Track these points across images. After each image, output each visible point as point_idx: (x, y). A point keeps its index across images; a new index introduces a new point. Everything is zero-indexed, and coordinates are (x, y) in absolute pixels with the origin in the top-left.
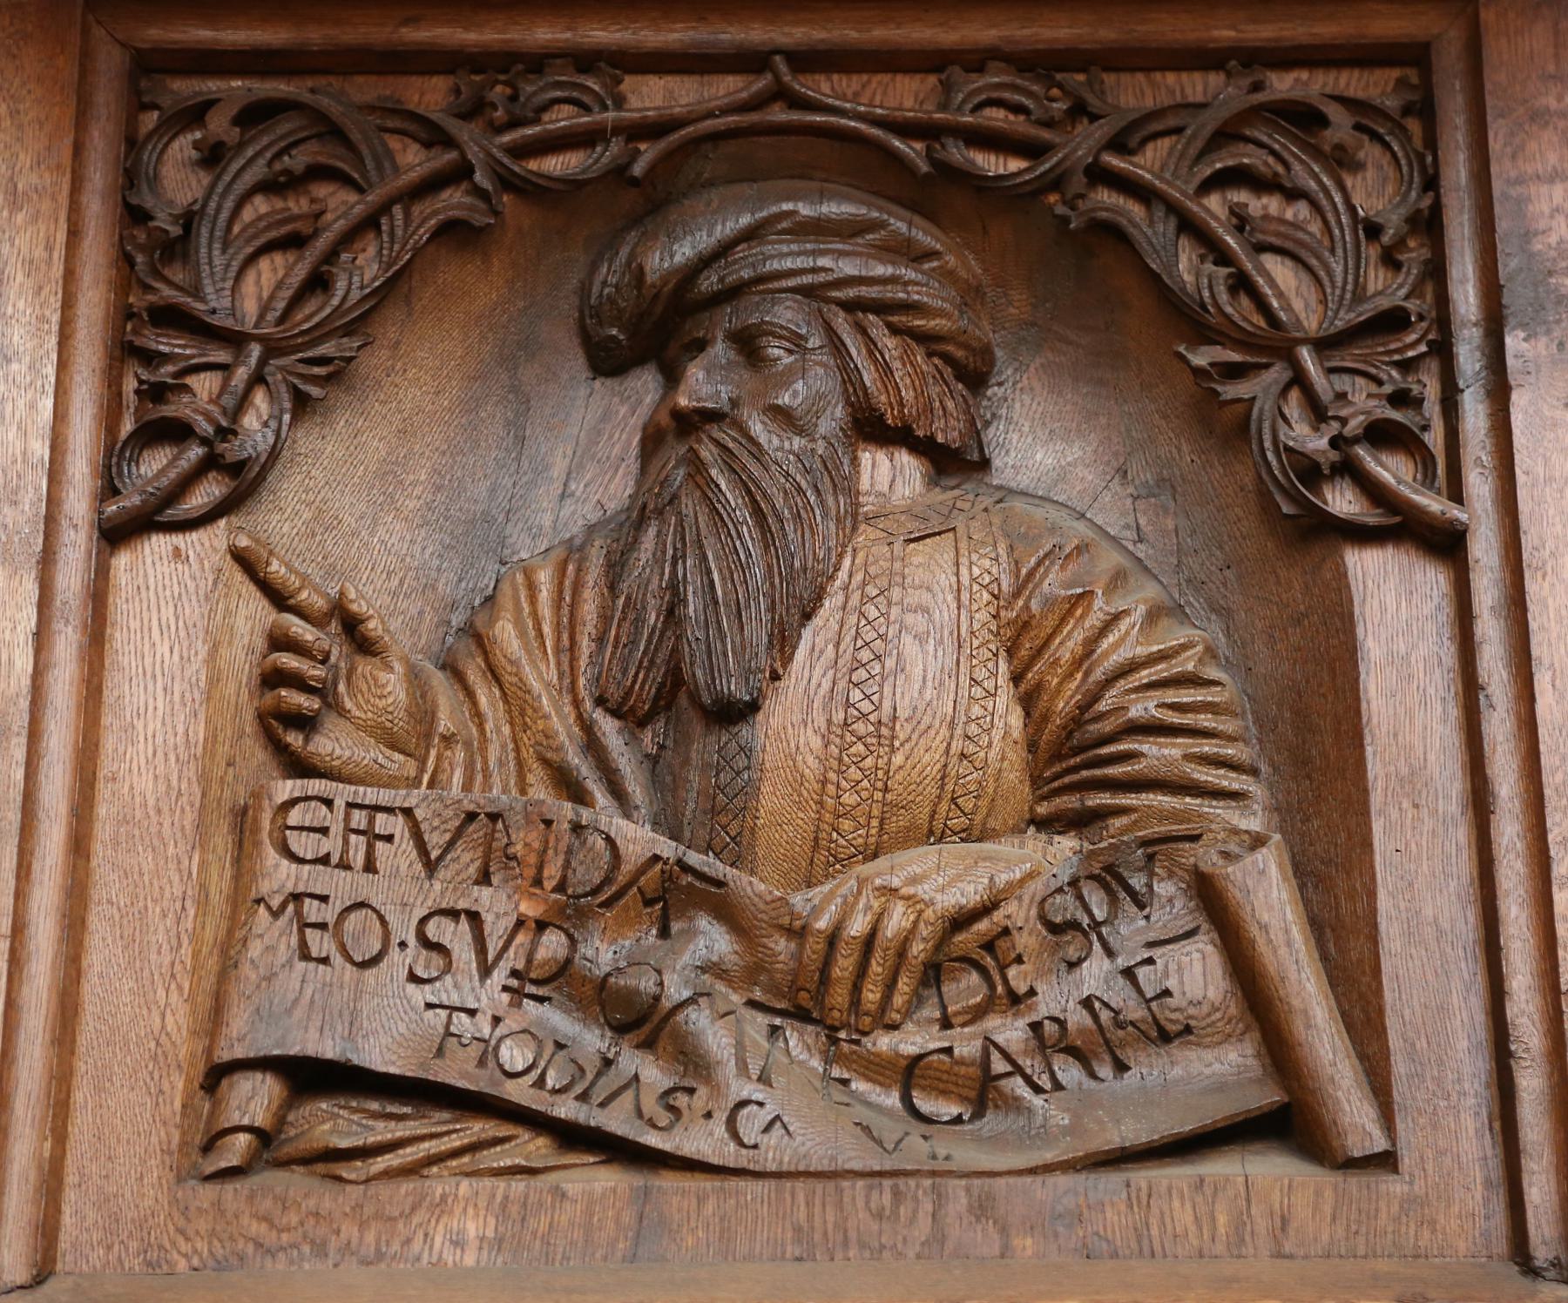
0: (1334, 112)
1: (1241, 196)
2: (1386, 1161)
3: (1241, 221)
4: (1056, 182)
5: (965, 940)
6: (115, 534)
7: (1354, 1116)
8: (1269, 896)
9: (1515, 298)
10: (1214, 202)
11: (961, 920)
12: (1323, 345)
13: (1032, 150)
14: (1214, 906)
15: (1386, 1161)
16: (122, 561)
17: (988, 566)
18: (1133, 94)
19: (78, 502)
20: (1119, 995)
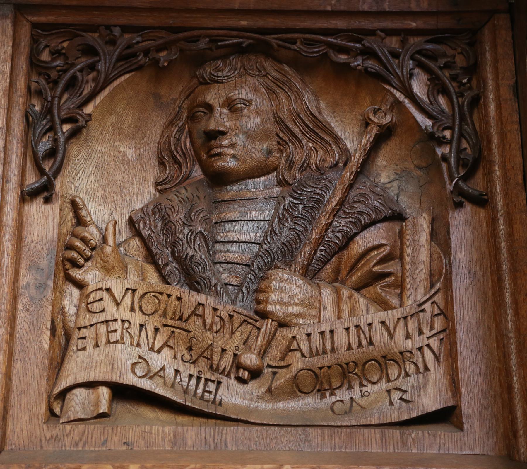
16: (27, 207)
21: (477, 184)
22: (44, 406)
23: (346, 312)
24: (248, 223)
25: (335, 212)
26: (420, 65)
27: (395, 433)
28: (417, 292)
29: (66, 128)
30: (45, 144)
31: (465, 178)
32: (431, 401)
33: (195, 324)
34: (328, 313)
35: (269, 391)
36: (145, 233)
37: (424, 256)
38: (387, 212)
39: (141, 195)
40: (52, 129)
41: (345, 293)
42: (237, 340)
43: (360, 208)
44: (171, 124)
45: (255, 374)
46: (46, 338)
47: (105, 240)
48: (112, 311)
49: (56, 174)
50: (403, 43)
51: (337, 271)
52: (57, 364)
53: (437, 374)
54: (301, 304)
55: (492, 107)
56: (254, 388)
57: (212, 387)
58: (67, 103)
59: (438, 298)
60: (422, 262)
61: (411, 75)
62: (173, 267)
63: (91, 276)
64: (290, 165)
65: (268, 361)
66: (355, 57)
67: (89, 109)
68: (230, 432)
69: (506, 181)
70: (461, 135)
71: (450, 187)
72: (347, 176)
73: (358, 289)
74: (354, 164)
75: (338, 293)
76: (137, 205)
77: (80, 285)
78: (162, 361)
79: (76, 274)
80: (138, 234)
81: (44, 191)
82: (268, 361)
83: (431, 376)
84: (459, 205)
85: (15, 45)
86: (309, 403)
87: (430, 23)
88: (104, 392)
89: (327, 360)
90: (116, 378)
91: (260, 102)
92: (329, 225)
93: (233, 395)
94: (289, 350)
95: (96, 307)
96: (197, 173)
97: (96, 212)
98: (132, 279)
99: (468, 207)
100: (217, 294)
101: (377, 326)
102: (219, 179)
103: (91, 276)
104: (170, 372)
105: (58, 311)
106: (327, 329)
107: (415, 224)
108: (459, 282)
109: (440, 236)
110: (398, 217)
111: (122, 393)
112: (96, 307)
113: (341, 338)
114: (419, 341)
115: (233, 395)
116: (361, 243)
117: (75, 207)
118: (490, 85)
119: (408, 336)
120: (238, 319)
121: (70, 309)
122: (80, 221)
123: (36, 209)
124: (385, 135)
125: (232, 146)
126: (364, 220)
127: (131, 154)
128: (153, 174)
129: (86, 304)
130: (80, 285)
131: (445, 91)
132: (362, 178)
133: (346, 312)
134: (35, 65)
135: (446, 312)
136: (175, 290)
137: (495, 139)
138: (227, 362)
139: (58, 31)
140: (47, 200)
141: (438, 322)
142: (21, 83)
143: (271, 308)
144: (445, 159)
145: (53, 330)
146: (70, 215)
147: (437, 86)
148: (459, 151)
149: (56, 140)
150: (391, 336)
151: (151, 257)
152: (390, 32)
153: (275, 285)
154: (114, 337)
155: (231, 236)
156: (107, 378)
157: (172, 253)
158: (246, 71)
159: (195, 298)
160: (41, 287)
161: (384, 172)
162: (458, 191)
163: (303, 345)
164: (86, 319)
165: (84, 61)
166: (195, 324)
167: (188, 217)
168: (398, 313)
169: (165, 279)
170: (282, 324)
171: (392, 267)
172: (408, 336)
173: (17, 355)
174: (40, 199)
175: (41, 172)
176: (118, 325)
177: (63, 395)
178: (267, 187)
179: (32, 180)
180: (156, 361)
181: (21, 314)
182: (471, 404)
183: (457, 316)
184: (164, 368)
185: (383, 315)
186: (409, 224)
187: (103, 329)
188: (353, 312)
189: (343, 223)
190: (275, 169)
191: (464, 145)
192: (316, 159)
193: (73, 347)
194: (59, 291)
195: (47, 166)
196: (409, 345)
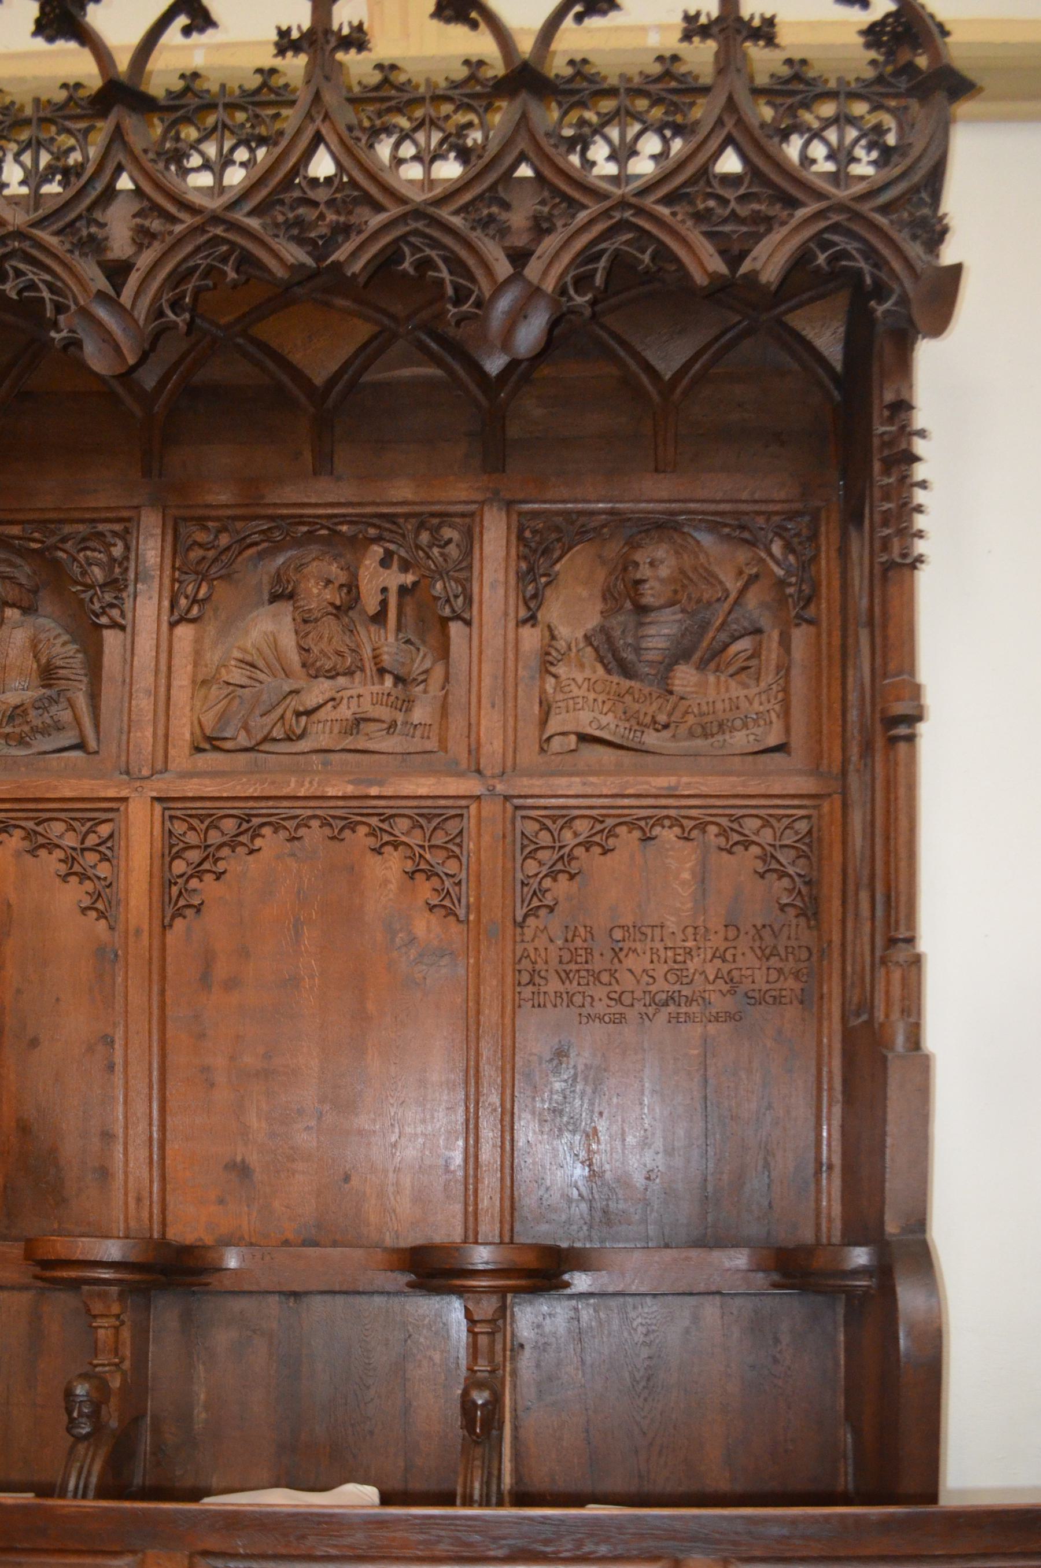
0: (108, 534)
1: (89, 553)
2: (97, 752)
3: (87, 558)
4: (48, 549)
5: (18, 711)
6: (172, 625)
7: (92, 744)
8: (82, 701)
9: (141, 576)
10: (81, 555)
11: (17, 707)
12: (100, 586)
13: (42, 542)
14: (72, 705)
15: (97, 752)
16: (520, 630)
17: (30, 632)
18: (67, 529)
19: (165, 618)
20: (49, 721)
21: (811, 612)
22: (537, 746)
23: (723, 690)
24: (661, 633)
25: (718, 630)
26: (777, 534)
27: (750, 758)
28: (769, 677)
29: (543, 580)
30: (531, 589)
31: (803, 608)
32: (772, 741)
33: (628, 699)
34: (712, 693)
35: (674, 736)
36: (595, 644)
37: (774, 656)
38: (751, 629)
39: (592, 621)
40: (534, 580)
41: (723, 678)
42: (655, 706)
43: (735, 626)
44: (610, 574)
45: (666, 727)
46: (536, 708)
47: (570, 649)
48: (576, 692)
49: (539, 607)
50: (768, 520)
51: (718, 666)
52: (544, 722)
53: (777, 725)
54: (695, 685)
55: (823, 563)
56: (666, 734)
57: (638, 734)
58: (543, 564)
59: (781, 681)
60: (507, 1499)
61: (771, 541)
62: (613, 665)
63: (561, 670)
64: (690, 598)
65: (673, 719)
66: (734, 530)
67: (558, 567)
68: (650, 758)
69: (829, 609)
70: (802, 581)
71: (793, 613)
72: (726, 606)
73: (731, 676)
74: (733, 595)
75: (718, 678)
76: (589, 626)
77: (555, 676)
78: (608, 719)
79: (553, 669)
80: (591, 644)
81: (531, 619)
82: (673, 719)
83: (774, 726)
84: (798, 625)
85: (509, 528)
86: (699, 743)
87: (786, 507)
88: (573, 738)
89: (710, 718)
90: (580, 730)
91: (672, 561)
92: (714, 638)
93: (651, 739)
94: (687, 712)
95: (567, 689)
96: (628, 605)
97: (563, 631)
98: (588, 673)
99: (804, 626)
100: (642, 681)
101: (742, 698)
102: (642, 610)
103: (561, 670)
104: (612, 726)
105: (543, 691)
106: (711, 700)
107: (769, 636)
108: (795, 672)
109: (785, 642)
110: (758, 631)
111: (584, 738)
112: (567, 689)
113: (719, 706)
114: (768, 707)
115: (651, 739)
116: (734, 648)
117: (550, 628)
118: (823, 548)
119: (761, 704)
120: (655, 695)
121: (550, 689)
122: (553, 637)
123: (526, 631)
124: (753, 579)
125: (652, 588)
126: (737, 634)
127: (585, 594)
128: (599, 606)
129: (559, 687)
130: (555, 676)
131: (793, 551)
132: (737, 608)
133: (723, 690)
134: (520, 537)
135: (786, 690)
136: (615, 679)
137: (824, 583)
138: (648, 720)
139: (825, 1142)
140: (533, 626)
141: (780, 696)
142: (513, 551)
143: (675, 688)
144: (791, 595)
145: (541, 703)
146: (547, 634)
147: (788, 548)
148: (800, 591)
149: (537, 589)
150: (751, 704)
151: (601, 659)
152: (758, 513)
153: (678, 674)
154: (579, 706)
155: (650, 645)
156: (574, 729)
157: (615, 658)
158: (661, 540)
159: (628, 683)
160: (533, 678)
161: (752, 600)
162: (798, 616)
163: (696, 710)
164: (560, 697)
165: (554, 536)
166: (628, 699)
167: (623, 632)
168: (756, 690)
169: (609, 672)
170: (682, 698)
171: (753, 662)
172: (761, 704)
173: (520, 718)
174: (528, 625)
175: (529, 609)
176: (580, 700)
177: (549, 739)
178: (674, 614)
179: (523, 613)
180: (604, 720)
181: (520, 693)
182: (797, 741)
183: (793, 691)
184: (606, 723)
185: (746, 692)
186: (765, 635)
187: (571, 702)
188: (727, 690)
189: (723, 637)
190: (679, 602)
191: (804, 587)
192: (706, 596)
193: (553, 713)
194: (543, 680)
195: (532, 605)
196: (761, 709)
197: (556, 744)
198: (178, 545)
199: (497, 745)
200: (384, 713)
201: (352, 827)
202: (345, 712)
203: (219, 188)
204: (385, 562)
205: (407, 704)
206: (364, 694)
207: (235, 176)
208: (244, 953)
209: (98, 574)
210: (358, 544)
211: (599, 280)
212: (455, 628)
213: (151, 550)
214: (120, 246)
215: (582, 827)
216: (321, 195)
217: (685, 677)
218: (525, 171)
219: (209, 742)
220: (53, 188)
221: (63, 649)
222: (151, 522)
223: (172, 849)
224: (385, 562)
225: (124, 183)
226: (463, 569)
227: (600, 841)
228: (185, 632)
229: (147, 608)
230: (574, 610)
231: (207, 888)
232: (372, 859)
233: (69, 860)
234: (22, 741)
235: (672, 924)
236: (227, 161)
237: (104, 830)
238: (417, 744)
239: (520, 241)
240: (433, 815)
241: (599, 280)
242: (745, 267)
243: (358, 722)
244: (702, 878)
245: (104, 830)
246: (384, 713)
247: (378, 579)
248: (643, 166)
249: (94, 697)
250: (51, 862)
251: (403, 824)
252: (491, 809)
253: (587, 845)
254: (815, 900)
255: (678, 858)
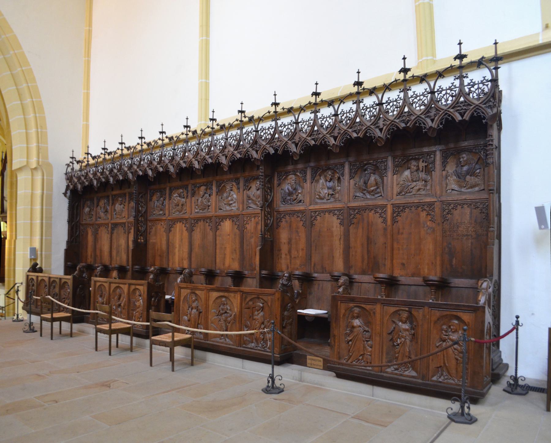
8: (381, 188)
32: (482, 189)
39: (454, 169)
81: (444, 170)
97: (450, 171)
103: (449, 178)
111: (452, 190)
115: (463, 190)
123: (443, 172)
197: (449, 191)
198: (394, 161)
199: (439, 192)
200: (423, 187)
201: (418, 207)
202: (417, 188)
203: (393, 115)
204: (423, 162)
205: (426, 186)
206: (420, 184)
207: (395, 113)
208: (404, 229)
209: (383, 168)
210: (418, 159)
211: (443, 123)
212: (433, 172)
213: (390, 163)
214: (381, 126)
215: (452, 205)
216: (406, 115)
217: (468, 177)
218: (433, 106)
219: (399, 194)
220: (373, 118)
221: (379, 180)
222: (390, 158)
223: (394, 212)
224: (423, 162)
225: (381, 116)
226: (434, 162)
227: (455, 208)
228: (395, 176)
229: (390, 174)
230: (451, 168)
231: (399, 218)
232: (421, 212)
233: (380, 215)
234: (373, 195)
235: (466, 222)
236: (394, 111)
237: (385, 209)
238: (428, 193)
239: (433, 118)
240: (431, 204)
241: (443, 123)
242: (464, 118)
243: (419, 189)
244: (471, 213)
245: (385, 209)
246: (423, 187)
247: (422, 165)
248: (449, 102)
249: (383, 187)
250: (378, 215)
251: (426, 206)
252: (438, 203)
253: (453, 209)
254: (488, 215)
255: (467, 211)
